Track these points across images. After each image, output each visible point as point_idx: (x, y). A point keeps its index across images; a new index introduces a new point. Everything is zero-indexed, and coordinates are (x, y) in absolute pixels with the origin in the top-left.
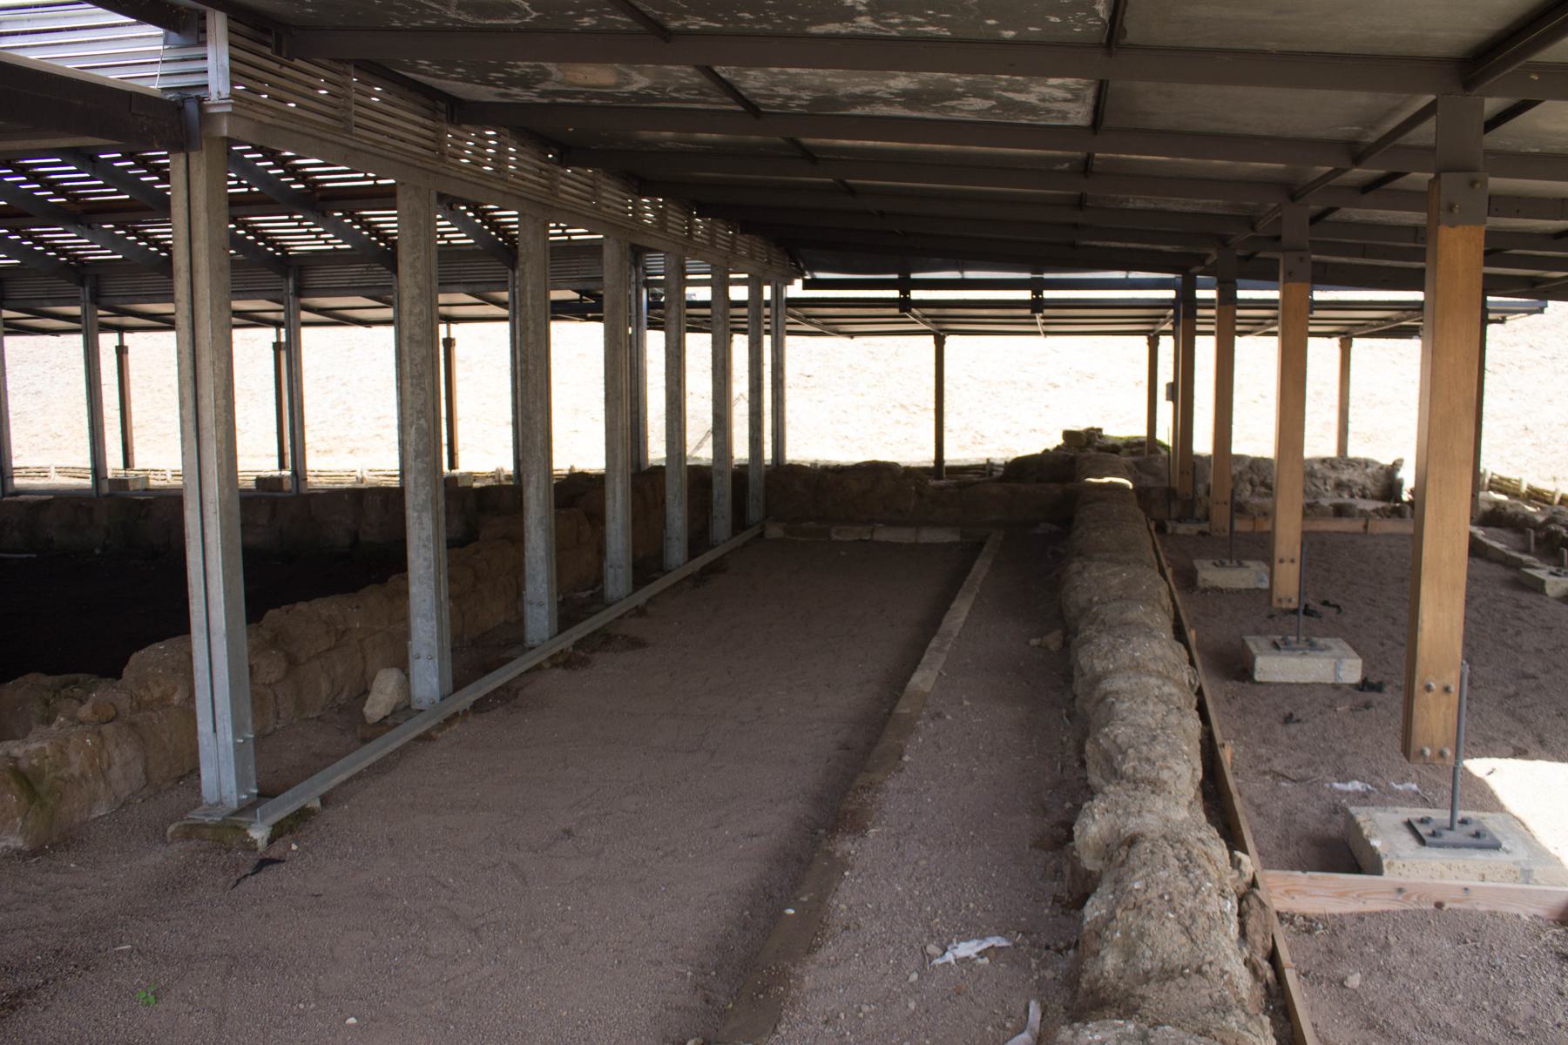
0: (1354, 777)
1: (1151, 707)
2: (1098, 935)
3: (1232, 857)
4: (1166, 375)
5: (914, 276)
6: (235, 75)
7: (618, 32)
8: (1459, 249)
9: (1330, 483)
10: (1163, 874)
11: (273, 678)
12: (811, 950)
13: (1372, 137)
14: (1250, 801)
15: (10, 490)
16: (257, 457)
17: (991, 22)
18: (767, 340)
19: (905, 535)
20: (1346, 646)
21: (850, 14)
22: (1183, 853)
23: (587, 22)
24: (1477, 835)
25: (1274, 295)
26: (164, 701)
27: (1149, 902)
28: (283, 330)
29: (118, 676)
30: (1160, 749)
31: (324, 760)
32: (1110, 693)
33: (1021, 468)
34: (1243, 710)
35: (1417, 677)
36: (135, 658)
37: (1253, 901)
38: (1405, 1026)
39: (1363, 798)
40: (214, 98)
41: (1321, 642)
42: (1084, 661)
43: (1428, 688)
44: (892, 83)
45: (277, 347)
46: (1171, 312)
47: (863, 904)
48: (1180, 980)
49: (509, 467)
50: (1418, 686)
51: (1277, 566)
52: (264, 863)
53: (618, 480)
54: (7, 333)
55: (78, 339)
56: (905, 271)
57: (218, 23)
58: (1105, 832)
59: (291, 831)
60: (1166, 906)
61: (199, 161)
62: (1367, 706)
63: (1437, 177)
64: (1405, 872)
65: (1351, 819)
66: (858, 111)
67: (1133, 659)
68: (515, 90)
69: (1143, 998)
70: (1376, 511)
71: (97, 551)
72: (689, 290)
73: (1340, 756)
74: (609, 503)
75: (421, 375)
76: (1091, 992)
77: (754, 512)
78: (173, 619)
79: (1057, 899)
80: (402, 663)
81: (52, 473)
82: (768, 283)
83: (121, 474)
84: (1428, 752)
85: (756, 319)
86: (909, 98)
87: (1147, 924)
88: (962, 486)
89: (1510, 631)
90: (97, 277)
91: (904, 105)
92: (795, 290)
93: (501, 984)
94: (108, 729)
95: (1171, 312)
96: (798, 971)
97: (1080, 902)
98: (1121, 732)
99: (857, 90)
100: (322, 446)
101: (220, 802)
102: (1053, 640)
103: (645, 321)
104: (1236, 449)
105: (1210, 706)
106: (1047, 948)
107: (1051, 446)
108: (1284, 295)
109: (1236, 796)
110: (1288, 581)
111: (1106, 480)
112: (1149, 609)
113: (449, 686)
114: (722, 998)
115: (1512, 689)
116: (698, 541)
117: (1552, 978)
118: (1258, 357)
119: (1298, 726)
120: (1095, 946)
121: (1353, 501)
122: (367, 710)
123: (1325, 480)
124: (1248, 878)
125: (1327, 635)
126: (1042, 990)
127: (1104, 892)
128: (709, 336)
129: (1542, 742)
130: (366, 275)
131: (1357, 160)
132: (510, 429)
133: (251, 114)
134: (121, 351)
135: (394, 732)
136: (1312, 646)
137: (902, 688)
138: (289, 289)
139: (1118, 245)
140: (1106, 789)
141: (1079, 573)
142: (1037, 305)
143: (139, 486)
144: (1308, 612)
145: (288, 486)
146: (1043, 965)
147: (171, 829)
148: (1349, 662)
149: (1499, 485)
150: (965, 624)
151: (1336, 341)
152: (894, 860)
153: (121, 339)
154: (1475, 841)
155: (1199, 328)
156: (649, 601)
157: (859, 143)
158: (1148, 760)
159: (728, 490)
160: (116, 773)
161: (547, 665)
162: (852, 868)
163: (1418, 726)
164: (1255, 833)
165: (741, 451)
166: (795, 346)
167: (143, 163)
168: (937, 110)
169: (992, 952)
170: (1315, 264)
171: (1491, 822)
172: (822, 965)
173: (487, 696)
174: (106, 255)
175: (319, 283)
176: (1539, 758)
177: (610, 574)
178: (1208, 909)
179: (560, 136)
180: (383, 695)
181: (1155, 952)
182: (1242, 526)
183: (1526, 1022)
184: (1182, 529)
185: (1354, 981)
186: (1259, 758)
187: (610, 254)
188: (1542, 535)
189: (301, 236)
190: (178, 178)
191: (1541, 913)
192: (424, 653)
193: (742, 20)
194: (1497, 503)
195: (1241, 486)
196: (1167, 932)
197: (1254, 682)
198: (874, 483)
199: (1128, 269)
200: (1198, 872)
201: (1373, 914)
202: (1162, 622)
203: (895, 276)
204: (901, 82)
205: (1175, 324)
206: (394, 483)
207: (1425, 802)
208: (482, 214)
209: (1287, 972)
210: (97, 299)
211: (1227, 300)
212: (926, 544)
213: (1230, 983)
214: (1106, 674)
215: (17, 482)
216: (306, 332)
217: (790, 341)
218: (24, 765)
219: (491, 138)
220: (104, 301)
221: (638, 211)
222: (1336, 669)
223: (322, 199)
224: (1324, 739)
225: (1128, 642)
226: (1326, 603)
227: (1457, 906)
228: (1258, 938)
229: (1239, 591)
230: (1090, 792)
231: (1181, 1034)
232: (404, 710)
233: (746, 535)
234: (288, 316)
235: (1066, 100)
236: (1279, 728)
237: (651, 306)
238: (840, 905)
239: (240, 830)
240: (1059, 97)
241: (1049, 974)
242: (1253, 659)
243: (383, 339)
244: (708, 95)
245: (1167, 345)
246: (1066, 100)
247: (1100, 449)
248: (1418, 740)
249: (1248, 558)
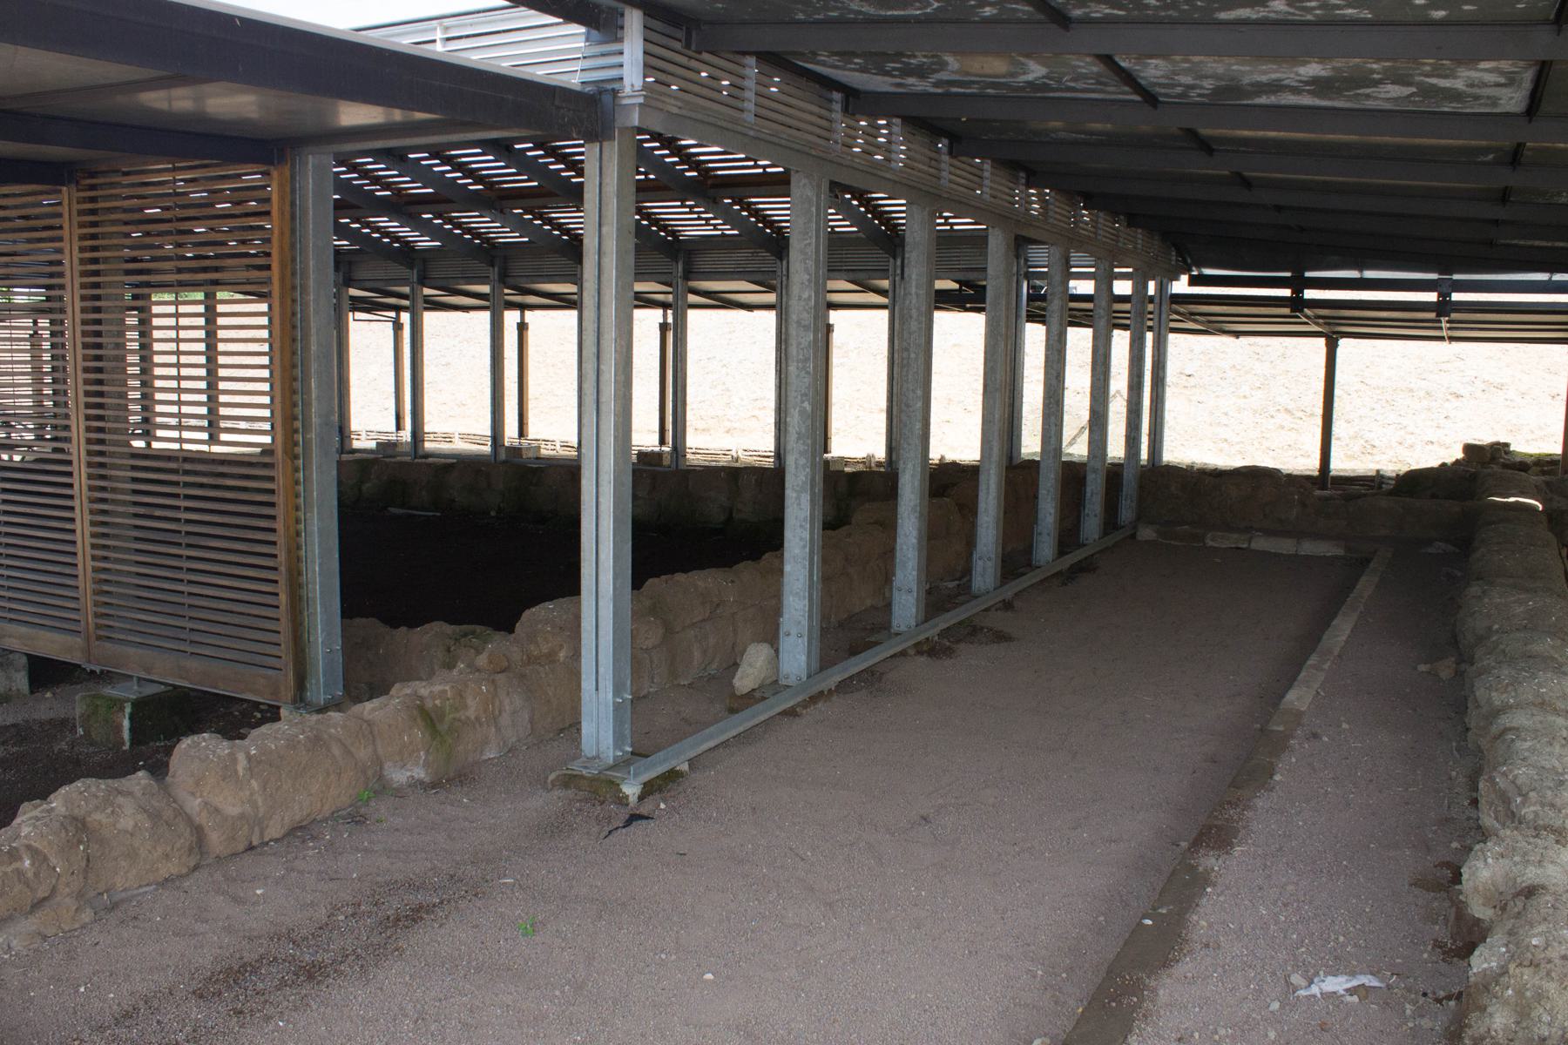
2: (1486, 988)
5: (1308, 274)
6: (648, 68)
7: (1020, 22)
11: (649, 643)
12: (1166, 964)
15: (420, 452)
16: (645, 436)
18: (1149, 336)
19: (1285, 546)
23: (988, 11)
26: (551, 657)
27: (1550, 961)
28: (670, 312)
29: (511, 631)
31: (692, 726)
32: (1510, 729)
33: (1414, 482)
36: (526, 614)
40: (628, 90)
42: (1480, 693)
44: (1302, 70)
45: (664, 327)
49: (880, 453)
52: (634, 818)
54: (427, 309)
55: (486, 316)
57: (634, 21)
59: (660, 790)
61: (613, 149)
66: (1263, 100)
68: (911, 80)
71: (493, 514)
72: (1072, 283)
75: (806, 360)
77: (1126, 513)
78: (567, 582)
79: (1438, 944)
80: (771, 636)
81: (456, 440)
83: (516, 443)
85: (1142, 314)
86: (1320, 86)
88: (1350, 498)
90: (350, 263)
92: (1181, 286)
93: (853, 960)
94: (501, 678)
96: (1153, 983)
97: (1467, 950)
98: (1522, 773)
99: (1264, 78)
100: (701, 425)
101: (598, 757)
102: (1446, 670)
103: (1024, 314)
106: (1425, 995)
107: (1450, 460)
111: (1512, 499)
112: (1559, 642)
113: (815, 665)
114: (1072, 1003)
116: (1068, 538)
120: (1485, 1000)
122: (737, 682)
130: (752, 260)
132: (884, 416)
133: (660, 105)
134: (522, 327)
135: (760, 706)
138: (675, 270)
140: (1502, 833)
143: (531, 455)
145: (666, 461)
146: (1420, 1013)
147: (552, 777)
150: (1347, 642)
153: (522, 316)
158: (1552, 805)
160: (505, 720)
161: (911, 652)
162: (1214, 885)
165: (1116, 449)
167: (553, 152)
168: (1349, 99)
173: (851, 678)
174: (514, 237)
175: (707, 268)
179: (939, 123)
180: (752, 670)
181: (1554, 1018)
187: (997, 243)
189: (692, 222)
190: (591, 168)
192: (794, 631)
199: (1552, 271)
203: (1288, 274)
206: (769, 463)
208: (867, 202)
210: (504, 279)
212: (1307, 557)
215: (428, 445)
216: (692, 314)
218: (429, 704)
219: (883, 127)
220: (511, 281)
223: (714, 186)
225: (1534, 676)
230: (1484, 835)
232: (773, 686)
234: (676, 298)
235: (1498, 85)
237: (1030, 298)
239: (614, 785)
243: (767, 321)
244: (1105, 84)
246: (1498, 85)
247: (1505, 466)
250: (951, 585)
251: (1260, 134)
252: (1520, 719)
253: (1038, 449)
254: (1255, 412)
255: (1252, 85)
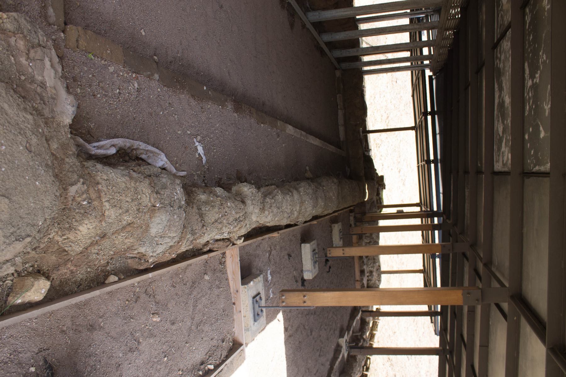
0: (272, 277)
1: (289, 207)
2: (211, 192)
3: (242, 236)
4: (406, 210)
5: (436, 116)
8: (455, 297)
9: (372, 269)
10: (233, 212)
12: (193, 96)
13: (493, 269)
14: (261, 243)
17: (531, 129)
19: (341, 121)
20: (316, 274)
21: (532, 77)
22: (241, 219)
24: (258, 315)
25: (437, 241)
30: (275, 210)
33: (369, 161)
34: (291, 240)
35: (308, 293)
37: (228, 243)
38: (195, 293)
39: (266, 280)
41: (317, 266)
42: (303, 184)
43: (304, 296)
44: (507, 97)
46: (429, 210)
47: (211, 113)
48: (200, 220)
50: (305, 293)
51: (342, 249)
53: (352, 12)
56: (438, 113)
58: (245, 193)
60: (223, 214)
62: (297, 281)
63: (480, 289)
64: (244, 292)
65: (259, 275)
66: (496, 86)
67: (305, 201)
69: (193, 207)
70: (363, 284)
72: (425, 32)
73: (279, 273)
74: (343, 10)
76: (192, 192)
77: (344, 65)
79: (221, 179)
82: (430, 62)
84: (283, 298)
85: (416, 59)
86: (502, 104)
87: (217, 208)
89: (326, 327)
91: (499, 103)
92: (428, 73)
95: (429, 210)
98: (280, 197)
99: (504, 85)
102: (309, 174)
103: (412, 17)
104: (382, 234)
105: (291, 229)
106: (204, 177)
107: (377, 172)
108: (437, 245)
109: (262, 238)
110: (337, 253)
111: (367, 191)
112: (323, 207)
115: (307, 327)
116: (332, 45)
117: (216, 337)
118: (415, 238)
119: (287, 258)
121: (366, 277)
123: (373, 267)
124: (235, 242)
125: (319, 268)
126: (190, 175)
127: (226, 194)
128: (408, 41)
129: (290, 336)
131: (485, 265)
136: (315, 262)
137: (286, 123)
139: (452, 188)
140: (260, 193)
141: (333, 182)
142: (428, 162)
144: (327, 261)
146: (199, 176)
148: (311, 274)
149: (375, 324)
151: (422, 268)
152: (227, 123)
154: (256, 314)
155: (424, 219)
156: (308, 29)
157: (484, 88)
159: (351, 55)
162: (222, 108)
163: (291, 294)
164: (250, 245)
166: (407, 75)
168: (497, 115)
169: (200, 158)
170: (449, 255)
171: (263, 319)
172: (188, 100)
176: (285, 335)
177: (316, 13)
178: (224, 228)
181: (208, 211)
182: (355, 238)
183: (202, 329)
184: (352, 218)
185: (207, 277)
186: (275, 246)
188: (359, 337)
191: (236, 334)
193: (530, 36)
194: (369, 323)
195: (368, 239)
196: (215, 215)
197: (301, 244)
198: (360, 109)
199: (443, 194)
200: (236, 224)
201: (228, 283)
202: (318, 211)
203: (436, 109)
204: (508, 100)
205: (424, 211)
207: (267, 300)
209: (207, 255)
211: (434, 227)
213: (201, 236)
214: (299, 192)
217: (409, 73)
221: (454, 8)
222: (308, 271)
224: (284, 267)
225: (311, 199)
226: (330, 267)
227: (235, 309)
228: (216, 246)
229: (332, 238)
230: (258, 188)
231: (183, 219)
233: (335, 63)
235: (503, 161)
236: (286, 252)
237: (418, 18)
238: (209, 105)
240: (504, 158)
241: (196, 178)
242: (309, 243)
245: (417, 209)
246: (503, 161)
247: (378, 189)
248: (287, 294)
249: (343, 241)
250: (308, 5)
251: (484, 88)
252: (296, 196)
253: (362, 29)
254: (386, 106)
255: (502, 81)
